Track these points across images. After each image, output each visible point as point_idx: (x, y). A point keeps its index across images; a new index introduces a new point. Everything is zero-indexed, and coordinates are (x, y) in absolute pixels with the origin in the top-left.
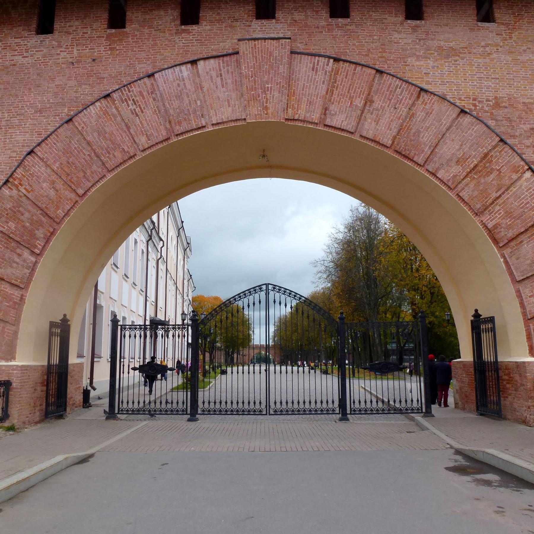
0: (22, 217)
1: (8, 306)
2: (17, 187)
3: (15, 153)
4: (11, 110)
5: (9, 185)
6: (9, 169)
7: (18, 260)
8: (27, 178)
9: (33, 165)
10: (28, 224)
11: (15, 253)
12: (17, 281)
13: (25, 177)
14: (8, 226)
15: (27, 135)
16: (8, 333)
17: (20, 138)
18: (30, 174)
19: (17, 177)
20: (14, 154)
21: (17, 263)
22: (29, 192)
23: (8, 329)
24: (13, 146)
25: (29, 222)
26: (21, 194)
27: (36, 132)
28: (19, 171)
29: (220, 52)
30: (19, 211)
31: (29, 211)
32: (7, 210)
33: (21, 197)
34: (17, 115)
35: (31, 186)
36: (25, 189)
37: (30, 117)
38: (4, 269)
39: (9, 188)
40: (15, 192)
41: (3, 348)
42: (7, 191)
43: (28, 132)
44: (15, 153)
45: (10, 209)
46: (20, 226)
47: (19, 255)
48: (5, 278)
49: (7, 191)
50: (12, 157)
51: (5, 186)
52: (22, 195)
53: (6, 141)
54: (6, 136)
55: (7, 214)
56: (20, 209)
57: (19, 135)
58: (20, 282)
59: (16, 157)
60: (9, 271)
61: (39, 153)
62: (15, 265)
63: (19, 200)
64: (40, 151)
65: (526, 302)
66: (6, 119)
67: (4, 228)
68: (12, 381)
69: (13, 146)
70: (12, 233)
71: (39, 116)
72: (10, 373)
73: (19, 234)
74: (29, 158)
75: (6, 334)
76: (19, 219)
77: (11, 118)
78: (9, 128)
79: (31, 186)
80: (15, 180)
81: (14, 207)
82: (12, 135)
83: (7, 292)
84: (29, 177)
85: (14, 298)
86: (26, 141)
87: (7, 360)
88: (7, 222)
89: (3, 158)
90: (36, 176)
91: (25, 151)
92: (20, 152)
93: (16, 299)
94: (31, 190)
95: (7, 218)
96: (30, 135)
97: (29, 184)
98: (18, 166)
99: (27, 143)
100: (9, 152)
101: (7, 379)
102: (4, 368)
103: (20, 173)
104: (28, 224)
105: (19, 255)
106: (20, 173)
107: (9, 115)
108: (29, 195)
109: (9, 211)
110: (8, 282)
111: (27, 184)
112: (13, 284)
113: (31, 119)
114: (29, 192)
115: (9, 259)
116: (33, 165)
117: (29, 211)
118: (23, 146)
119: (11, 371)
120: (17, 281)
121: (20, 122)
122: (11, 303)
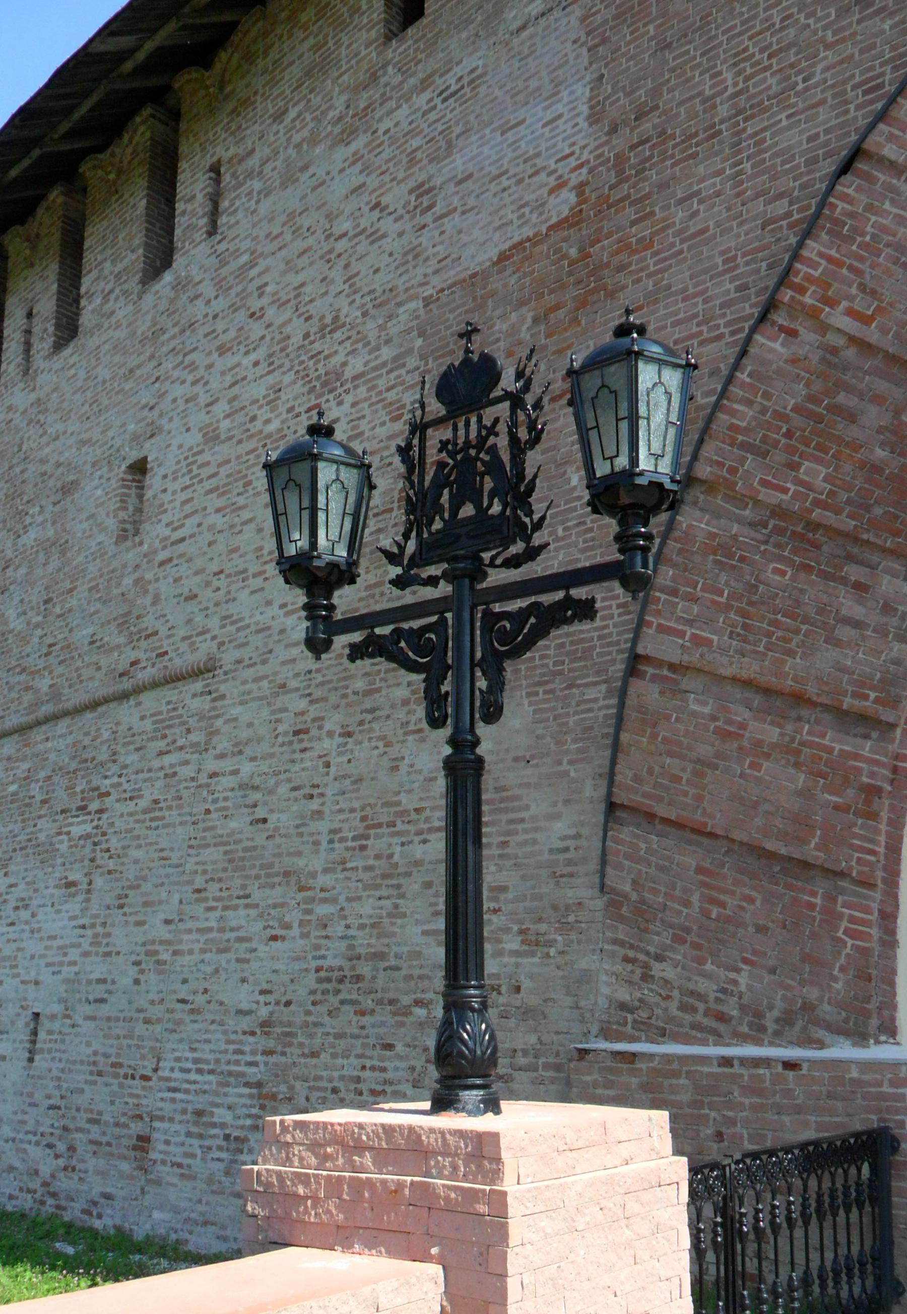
0: (852, 432)
1: (837, 807)
2: (813, 314)
3: (786, 201)
4: (746, 50)
5: (780, 318)
6: (770, 267)
7: (857, 611)
8: (851, 268)
9: (869, 208)
10: (880, 453)
11: (844, 581)
12: (866, 697)
13: (839, 264)
14: (798, 482)
15: (823, 114)
16: (852, 920)
17: (795, 138)
18: (863, 246)
19: (808, 278)
20: (781, 207)
21: (858, 625)
22: (866, 320)
23: (846, 905)
24: (773, 178)
25: (882, 445)
26: (833, 339)
27: (854, 88)
28: (812, 250)
29: (567, 635)
30: (835, 409)
31: (878, 399)
32: (783, 418)
33: (834, 351)
34: (770, 57)
35: (873, 293)
36: (850, 312)
37: (822, 40)
38: (804, 656)
39: (782, 329)
40: (808, 335)
41: (838, 986)
42: (777, 346)
43: (822, 102)
44: (786, 201)
45: (796, 409)
46: (847, 467)
47: (860, 587)
48: (812, 690)
49: (777, 346)
50: (774, 220)
51: (766, 327)
52: (841, 342)
53: (740, 173)
54: (739, 152)
55: (789, 434)
56: (841, 398)
57: (789, 128)
58: (877, 700)
59: (789, 214)
60: (826, 659)
61: (889, 151)
62: (845, 633)
63: (829, 364)
64: (891, 138)
65: (436, 895)
66: (730, 91)
67: (785, 491)
68: (896, 1132)
69: (773, 178)
70: (817, 503)
71: (859, 22)
72: (883, 1097)
73: (849, 502)
74: (849, 186)
75: (844, 924)
76: (839, 440)
77: (747, 79)
78: (746, 120)
79: (873, 293)
80: (802, 290)
81: (811, 398)
82: (764, 140)
83: (830, 751)
84: (861, 259)
85: (859, 770)
86: (822, 138)
87: (861, 1037)
88: (794, 467)
89: (738, 235)
90: (888, 245)
91: (821, 180)
92: (803, 187)
93: (872, 775)
94: (879, 310)
95: (790, 450)
96: (833, 108)
97: (862, 288)
98: (807, 234)
99: (827, 143)
100: (759, 206)
101: (873, 1121)
102: (855, 1074)
103: (821, 255)
104: (880, 453)
105: (860, 587)
106: (821, 255)
107: (739, 73)
108: (872, 334)
109: (797, 421)
110: (826, 708)
111: (854, 290)
112: (846, 713)
113: (828, 47)
114: (866, 320)
115: (821, 611)
116: (869, 208)
117: (878, 399)
118: (814, 161)
119: (886, 1089)
120: (866, 697)
121: (788, 78)
122: (850, 792)
